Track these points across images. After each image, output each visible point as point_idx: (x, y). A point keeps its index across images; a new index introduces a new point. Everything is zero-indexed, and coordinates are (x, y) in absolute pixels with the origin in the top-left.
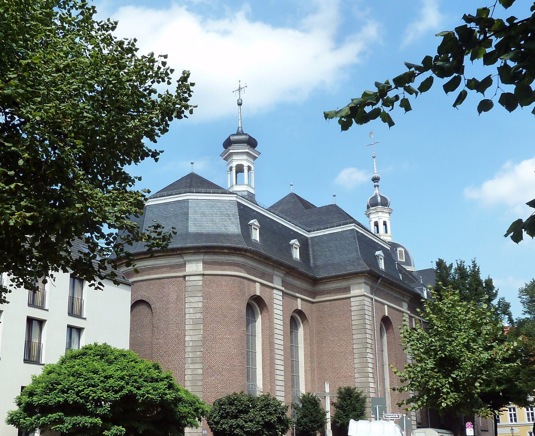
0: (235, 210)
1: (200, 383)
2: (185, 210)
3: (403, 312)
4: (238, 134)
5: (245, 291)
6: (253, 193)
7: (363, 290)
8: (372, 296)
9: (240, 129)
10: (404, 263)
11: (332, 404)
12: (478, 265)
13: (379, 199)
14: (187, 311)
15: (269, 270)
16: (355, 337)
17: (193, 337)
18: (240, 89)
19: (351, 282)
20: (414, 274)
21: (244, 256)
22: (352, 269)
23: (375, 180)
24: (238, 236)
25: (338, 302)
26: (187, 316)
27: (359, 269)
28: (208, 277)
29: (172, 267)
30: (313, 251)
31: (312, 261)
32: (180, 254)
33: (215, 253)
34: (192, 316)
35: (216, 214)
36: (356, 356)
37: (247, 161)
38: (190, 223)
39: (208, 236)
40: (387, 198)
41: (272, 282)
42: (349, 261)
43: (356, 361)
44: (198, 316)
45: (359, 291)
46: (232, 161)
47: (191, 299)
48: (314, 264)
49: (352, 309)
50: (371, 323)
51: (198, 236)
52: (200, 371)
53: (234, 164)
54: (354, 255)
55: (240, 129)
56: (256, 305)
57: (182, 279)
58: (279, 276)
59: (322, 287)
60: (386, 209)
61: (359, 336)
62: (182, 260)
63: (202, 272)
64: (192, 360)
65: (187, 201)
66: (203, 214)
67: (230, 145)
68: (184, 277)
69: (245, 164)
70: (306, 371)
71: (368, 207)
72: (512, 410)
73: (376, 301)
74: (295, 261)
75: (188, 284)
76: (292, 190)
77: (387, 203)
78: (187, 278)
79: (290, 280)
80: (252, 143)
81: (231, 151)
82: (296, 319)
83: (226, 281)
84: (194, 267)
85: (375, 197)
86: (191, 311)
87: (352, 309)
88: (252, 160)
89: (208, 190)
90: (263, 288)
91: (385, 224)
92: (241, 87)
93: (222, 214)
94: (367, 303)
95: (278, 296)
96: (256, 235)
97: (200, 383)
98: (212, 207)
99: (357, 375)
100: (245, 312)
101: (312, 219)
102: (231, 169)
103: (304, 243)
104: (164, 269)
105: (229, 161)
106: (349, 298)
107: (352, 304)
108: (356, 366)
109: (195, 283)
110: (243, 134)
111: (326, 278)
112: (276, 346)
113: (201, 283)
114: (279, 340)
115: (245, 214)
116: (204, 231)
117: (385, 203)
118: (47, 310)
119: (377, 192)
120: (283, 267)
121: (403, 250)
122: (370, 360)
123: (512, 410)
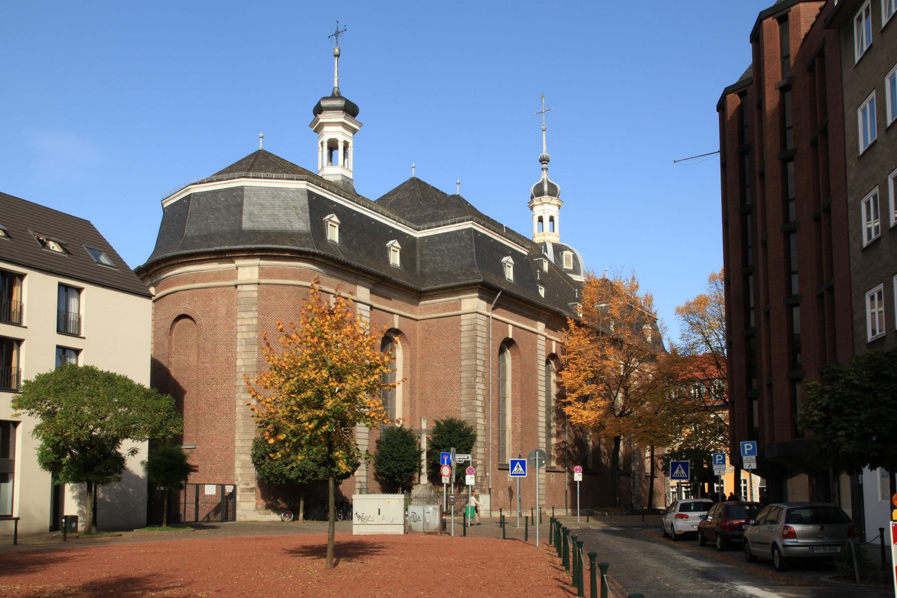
0: (305, 201)
2: (239, 200)
4: (333, 97)
6: (351, 177)
8: (489, 314)
10: (570, 271)
11: (428, 441)
12: (637, 278)
16: (463, 363)
18: (337, 34)
24: (306, 235)
26: (239, 336)
30: (422, 255)
31: (418, 267)
34: (245, 336)
37: (343, 134)
42: (462, 268)
47: (244, 315)
50: (486, 344)
51: (254, 234)
55: (336, 90)
60: (555, 201)
63: (257, 281)
65: (241, 189)
67: (320, 113)
68: (236, 286)
70: (404, 404)
71: (532, 197)
74: (394, 269)
75: (240, 295)
76: (413, 174)
77: (557, 192)
81: (321, 121)
83: (288, 292)
91: (552, 219)
94: (480, 322)
96: (333, 234)
99: (463, 409)
102: (322, 143)
103: (409, 246)
107: (463, 323)
108: (462, 398)
109: (248, 294)
111: (432, 290)
113: (255, 294)
115: (318, 208)
117: (553, 191)
118: (26, 327)
121: (571, 254)
122: (479, 392)
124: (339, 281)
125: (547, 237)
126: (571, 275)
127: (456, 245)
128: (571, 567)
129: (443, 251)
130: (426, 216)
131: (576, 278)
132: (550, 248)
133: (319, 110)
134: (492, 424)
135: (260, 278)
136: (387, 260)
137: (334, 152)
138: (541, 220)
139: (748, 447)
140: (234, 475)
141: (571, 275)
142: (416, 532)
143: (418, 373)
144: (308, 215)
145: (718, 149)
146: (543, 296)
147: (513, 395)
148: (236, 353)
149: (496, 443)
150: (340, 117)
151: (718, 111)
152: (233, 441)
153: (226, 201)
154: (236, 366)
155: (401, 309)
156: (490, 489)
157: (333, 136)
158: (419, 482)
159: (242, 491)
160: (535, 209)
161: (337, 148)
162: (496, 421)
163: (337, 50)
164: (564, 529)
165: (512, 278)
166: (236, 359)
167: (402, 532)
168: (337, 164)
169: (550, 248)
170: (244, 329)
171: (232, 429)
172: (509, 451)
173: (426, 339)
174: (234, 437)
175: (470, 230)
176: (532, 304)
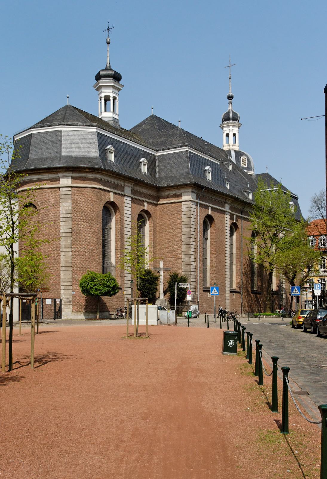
0: (95, 139)
1: (70, 261)
2: (59, 138)
3: (225, 211)
4: (106, 69)
5: (101, 199)
7: (190, 196)
8: (198, 201)
9: (108, 65)
10: (246, 169)
13: (231, 115)
14: (61, 212)
15: (120, 183)
17: (66, 230)
18: (108, 29)
19: (182, 191)
20: (254, 177)
21: (101, 174)
22: (183, 181)
23: (230, 97)
25: (173, 204)
26: (61, 216)
27: (188, 182)
28: (75, 188)
29: (52, 180)
30: (159, 166)
32: (56, 172)
33: (80, 172)
34: (65, 216)
35: (82, 141)
36: (184, 243)
37: (113, 92)
38: (63, 148)
39: (76, 159)
40: (237, 113)
41: (123, 191)
43: (183, 246)
44: (69, 216)
45: (188, 197)
46: (101, 93)
48: (159, 176)
49: (183, 210)
51: (69, 158)
52: (70, 253)
53: (103, 95)
54: (186, 170)
55: (108, 65)
56: (110, 209)
57: (57, 189)
58: (129, 186)
59: (163, 194)
61: (186, 229)
62: (57, 176)
63: (71, 185)
64: (65, 246)
65: (60, 131)
66: (72, 142)
68: (59, 188)
69: (112, 95)
71: (223, 121)
72: (323, 280)
73: (200, 204)
74: (144, 175)
75: (62, 193)
76: (152, 113)
77: (237, 118)
78: (61, 189)
79: (138, 188)
80: (117, 77)
81: (100, 84)
82: (142, 218)
84: (66, 181)
85: (228, 113)
86: (64, 212)
87: (183, 210)
88: (117, 92)
89: (76, 123)
90: (116, 196)
91: (234, 135)
92: (107, 32)
93: (86, 142)
95: (128, 201)
96: (111, 157)
97: (70, 261)
98: (79, 136)
99: (183, 256)
100: (101, 213)
101: (161, 140)
102: (101, 98)
103: (152, 162)
104: (45, 182)
105: (100, 91)
106: (181, 202)
107: (183, 207)
108: (183, 250)
109: (66, 193)
110: (111, 70)
111: (165, 187)
112: (126, 236)
114: (128, 232)
116: (73, 155)
117: (235, 118)
119: (230, 108)
120: (132, 180)
123: (323, 280)
124: (253, 354)
125: (232, 146)
126: (246, 171)
127: (179, 160)
128: (246, 349)
129: (171, 164)
130: (161, 142)
131: (249, 172)
132: (233, 153)
133: (99, 77)
134: (200, 265)
135: (72, 183)
136: (140, 170)
137: (107, 102)
138: (228, 135)
139: (317, 286)
140: (60, 293)
141: (246, 171)
142: (164, 324)
143: (158, 235)
144: (97, 146)
145: (325, 114)
146: (228, 188)
147: (211, 248)
148: (60, 225)
149: (202, 275)
150: (110, 82)
151: (324, 93)
152: (59, 275)
153: (52, 138)
154: (60, 233)
155: (148, 199)
156: (198, 302)
157: (107, 94)
158: (159, 298)
159: (65, 303)
160: (225, 129)
161: (110, 100)
162: (201, 263)
163: (108, 40)
164: (243, 327)
165: (210, 179)
166: (60, 229)
167: (156, 324)
168: (110, 111)
169: (233, 153)
170: (64, 212)
171: (59, 268)
172: (209, 280)
173: (162, 215)
174: (60, 273)
175: (186, 151)
176: (222, 194)
